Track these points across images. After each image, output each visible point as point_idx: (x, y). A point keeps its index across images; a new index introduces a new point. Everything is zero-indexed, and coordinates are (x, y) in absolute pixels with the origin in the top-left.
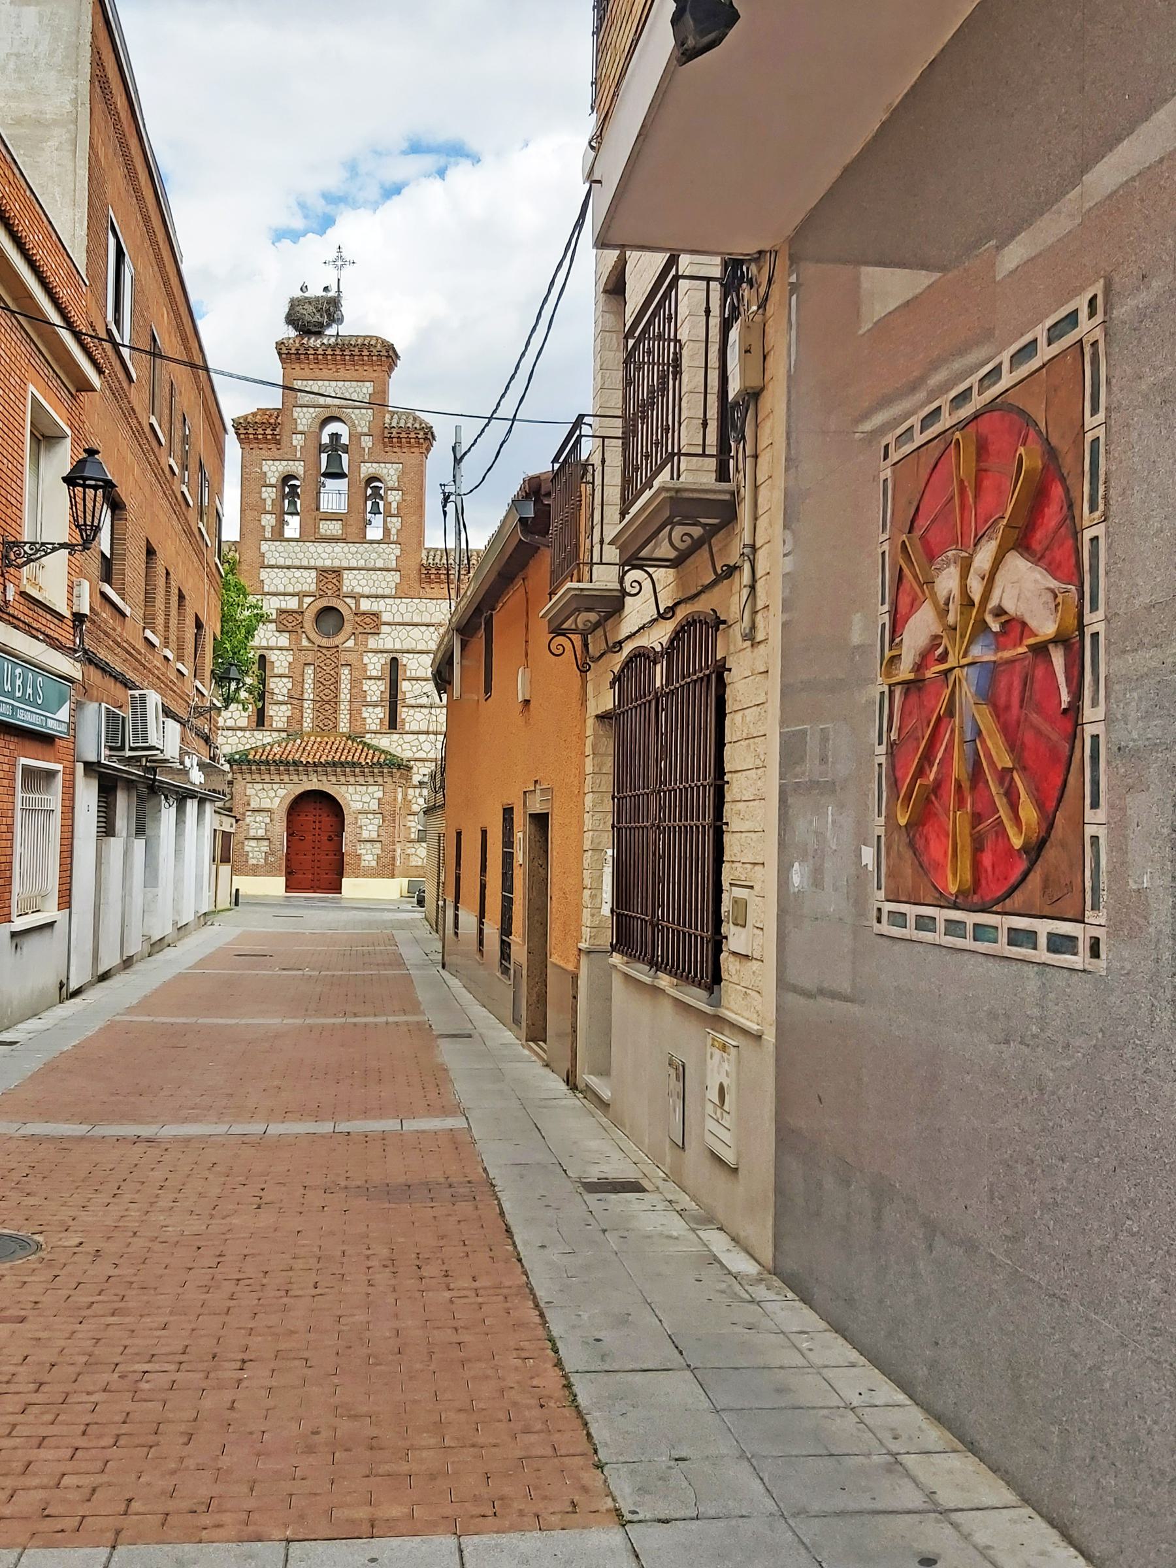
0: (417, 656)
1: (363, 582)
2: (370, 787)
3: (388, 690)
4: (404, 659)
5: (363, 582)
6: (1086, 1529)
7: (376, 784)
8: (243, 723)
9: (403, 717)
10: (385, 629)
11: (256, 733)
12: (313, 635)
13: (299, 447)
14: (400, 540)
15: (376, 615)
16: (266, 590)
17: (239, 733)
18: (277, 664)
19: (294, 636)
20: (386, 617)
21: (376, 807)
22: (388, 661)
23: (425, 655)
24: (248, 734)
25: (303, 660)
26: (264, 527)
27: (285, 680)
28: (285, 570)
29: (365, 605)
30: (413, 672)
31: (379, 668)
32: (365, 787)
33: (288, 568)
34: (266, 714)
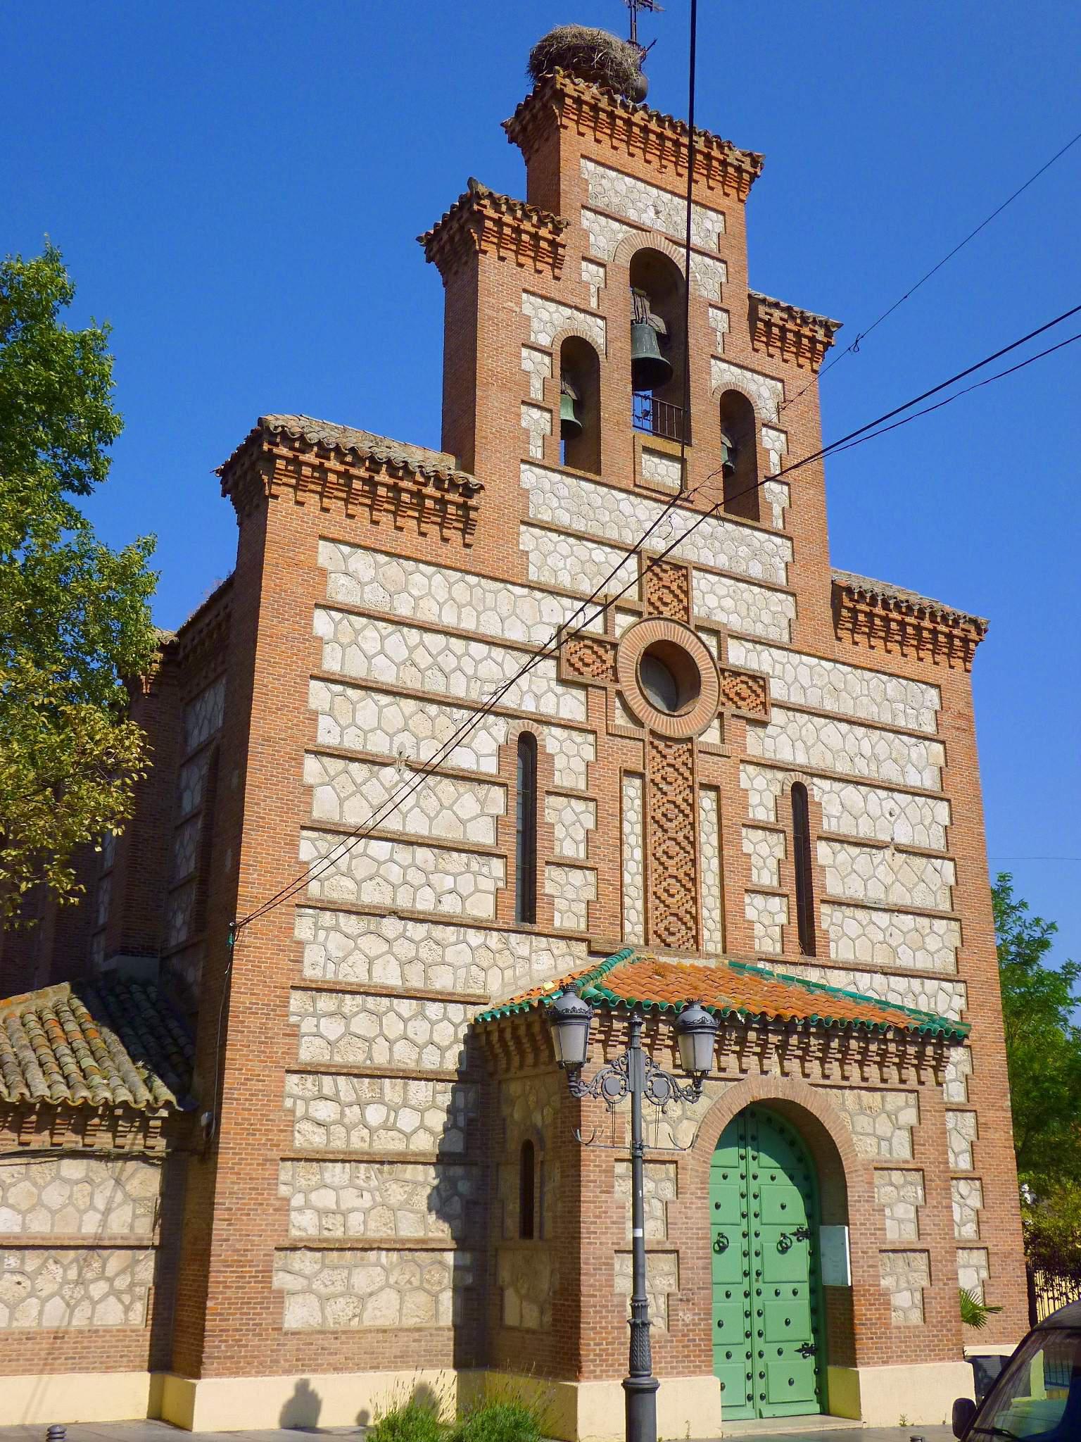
0: (838, 786)
1: (728, 603)
2: (890, 1096)
3: (792, 858)
4: (819, 790)
5: (728, 603)
6: (399, 1197)
7: (902, 1087)
8: (483, 908)
9: (824, 926)
10: (777, 715)
11: (514, 937)
12: (637, 703)
13: (593, 289)
14: (790, 531)
15: (758, 680)
16: (533, 575)
17: (474, 937)
18: (559, 762)
19: (597, 696)
20: (777, 690)
21: (905, 1153)
22: (788, 789)
23: (851, 787)
24: (494, 939)
25: (619, 761)
26: (527, 431)
27: (579, 806)
28: (572, 540)
29: (737, 655)
30: (834, 821)
31: (771, 805)
32: (878, 1095)
33: (580, 537)
34: (539, 891)
